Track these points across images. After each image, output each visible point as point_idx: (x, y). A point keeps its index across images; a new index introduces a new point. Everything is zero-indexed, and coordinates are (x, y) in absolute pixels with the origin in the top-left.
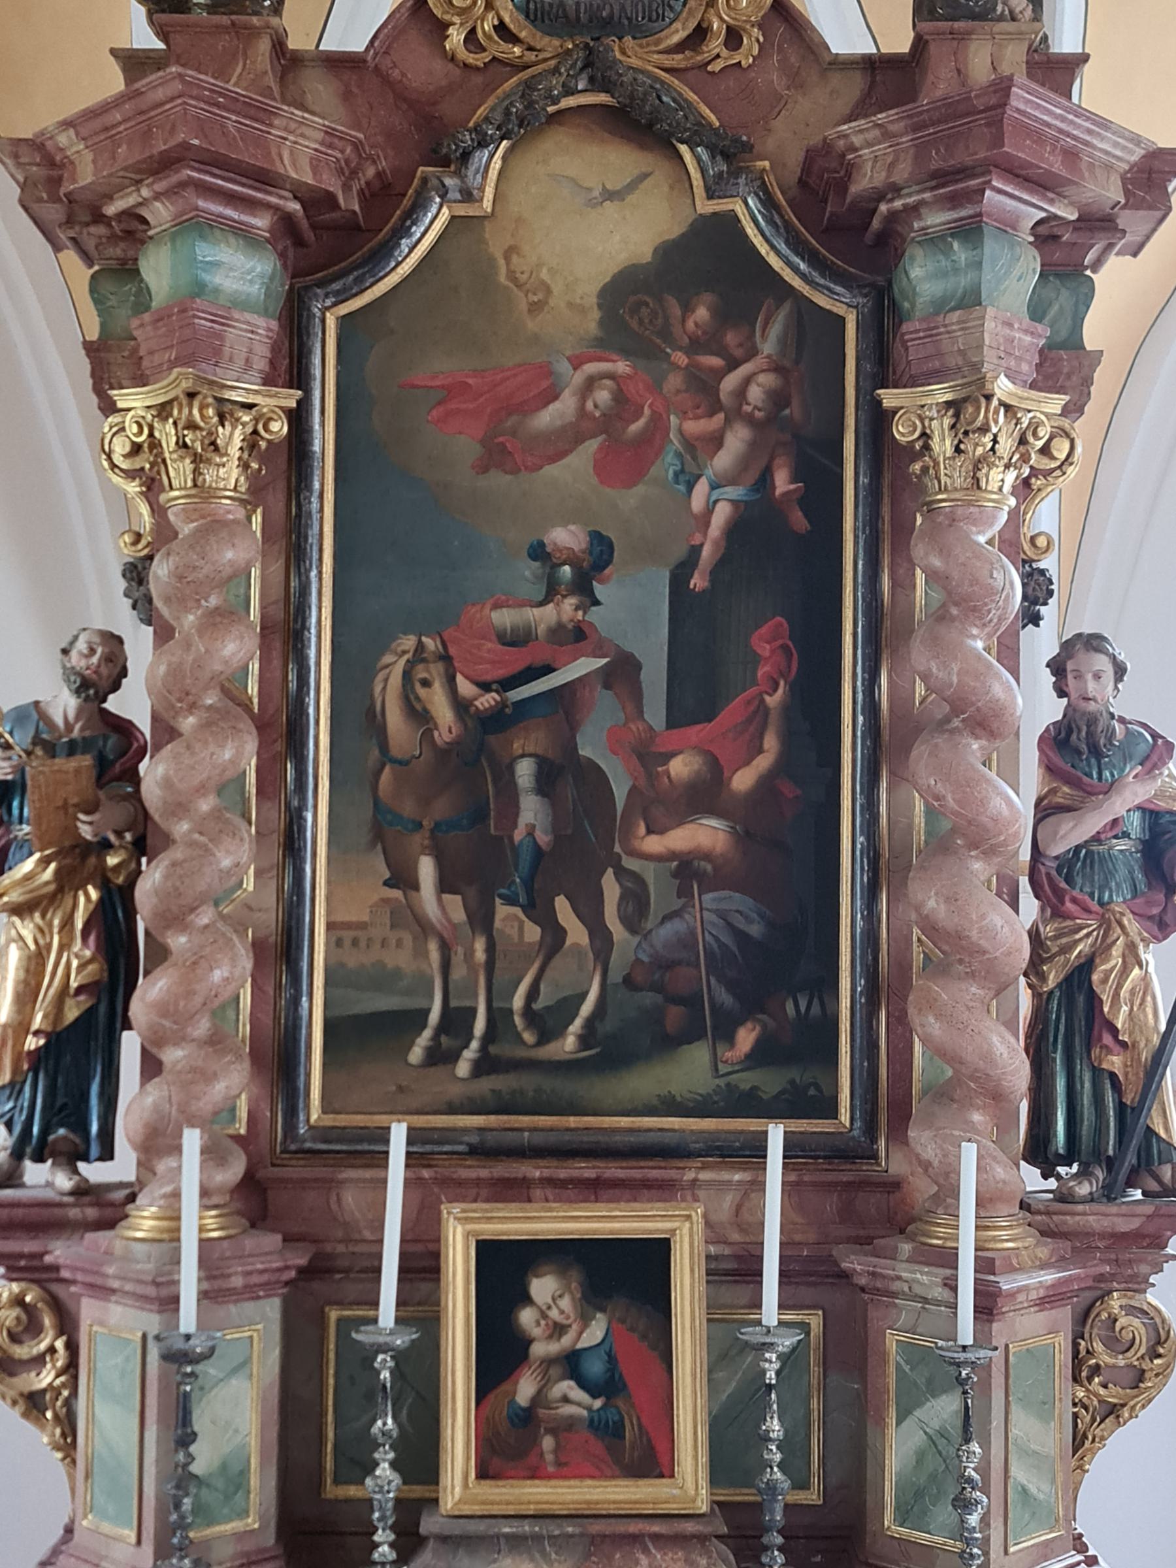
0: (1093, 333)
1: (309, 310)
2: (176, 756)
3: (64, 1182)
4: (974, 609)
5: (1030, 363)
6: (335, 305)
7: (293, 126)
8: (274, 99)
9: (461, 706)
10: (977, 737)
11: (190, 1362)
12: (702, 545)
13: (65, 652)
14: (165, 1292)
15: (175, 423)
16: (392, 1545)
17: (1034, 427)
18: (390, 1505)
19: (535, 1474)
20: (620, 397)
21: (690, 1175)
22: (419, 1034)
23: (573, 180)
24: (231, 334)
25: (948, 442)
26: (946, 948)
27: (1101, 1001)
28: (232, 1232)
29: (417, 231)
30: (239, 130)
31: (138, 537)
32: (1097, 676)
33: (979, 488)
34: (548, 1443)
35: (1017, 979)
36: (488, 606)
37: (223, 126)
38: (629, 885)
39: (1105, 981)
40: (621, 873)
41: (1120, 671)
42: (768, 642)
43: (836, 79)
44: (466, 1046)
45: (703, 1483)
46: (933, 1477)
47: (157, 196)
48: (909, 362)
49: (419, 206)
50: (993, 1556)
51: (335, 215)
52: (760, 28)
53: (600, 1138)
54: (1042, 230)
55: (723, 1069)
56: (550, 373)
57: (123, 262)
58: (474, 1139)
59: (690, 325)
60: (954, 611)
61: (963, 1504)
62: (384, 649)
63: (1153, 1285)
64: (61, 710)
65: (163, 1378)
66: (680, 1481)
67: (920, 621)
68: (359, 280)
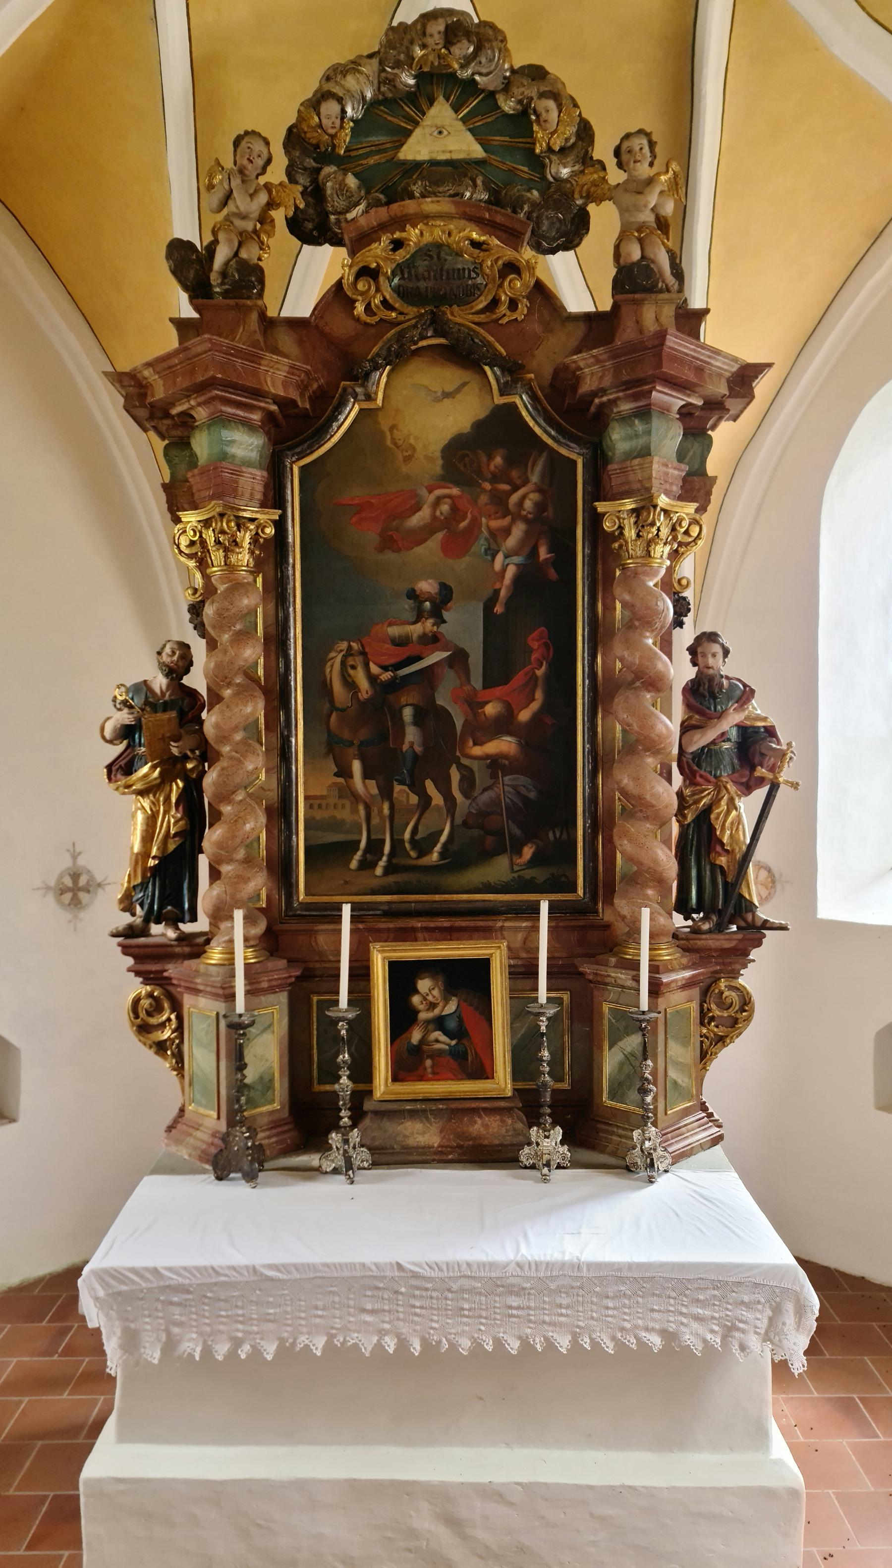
0: (712, 466)
1: (283, 463)
2: (222, 712)
3: (171, 934)
4: (648, 623)
5: (677, 485)
6: (298, 460)
7: (272, 364)
8: (262, 350)
9: (373, 679)
10: (649, 692)
11: (242, 1029)
12: (500, 589)
13: (159, 653)
14: (227, 992)
15: (213, 530)
16: (349, 1118)
17: (680, 521)
18: (348, 1097)
19: (422, 1078)
20: (454, 509)
21: (499, 924)
22: (355, 854)
23: (426, 387)
24: (242, 480)
25: (633, 531)
26: (633, 802)
27: (715, 829)
28: (261, 959)
29: (341, 418)
30: (242, 367)
31: (195, 591)
32: (714, 655)
33: (650, 556)
34: (428, 1063)
35: (671, 819)
36: (386, 624)
37: (234, 365)
38: (465, 773)
39: (717, 818)
40: (460, 767)
41: (726, 652)
42: (537, 641)
43: (570, 327)
44: (380, 859)
45: (509, 1081)
46: (628, 1076)
47: (199, 405)
48: (611, 487)
49: (341, 404)
50: (659, 1115)
51: (296, 411)
52: (528, 299)
53: (452, 906)
54: (684, 411)
55: (516, 868)
56: (417, 495)
57: (181, 438)
58: (386, 908)
59: (492, 467)
60: (637, 623)
61: (644, 1091)
62: (331, 649)
63: (753, 961)
64: (158, 686)
65: (228, 1035)
66: (497, 1081)
67: (618, 629)
68: (310, 447)
